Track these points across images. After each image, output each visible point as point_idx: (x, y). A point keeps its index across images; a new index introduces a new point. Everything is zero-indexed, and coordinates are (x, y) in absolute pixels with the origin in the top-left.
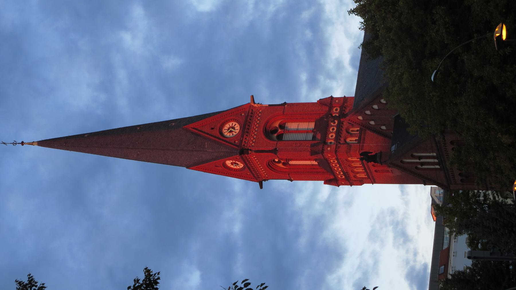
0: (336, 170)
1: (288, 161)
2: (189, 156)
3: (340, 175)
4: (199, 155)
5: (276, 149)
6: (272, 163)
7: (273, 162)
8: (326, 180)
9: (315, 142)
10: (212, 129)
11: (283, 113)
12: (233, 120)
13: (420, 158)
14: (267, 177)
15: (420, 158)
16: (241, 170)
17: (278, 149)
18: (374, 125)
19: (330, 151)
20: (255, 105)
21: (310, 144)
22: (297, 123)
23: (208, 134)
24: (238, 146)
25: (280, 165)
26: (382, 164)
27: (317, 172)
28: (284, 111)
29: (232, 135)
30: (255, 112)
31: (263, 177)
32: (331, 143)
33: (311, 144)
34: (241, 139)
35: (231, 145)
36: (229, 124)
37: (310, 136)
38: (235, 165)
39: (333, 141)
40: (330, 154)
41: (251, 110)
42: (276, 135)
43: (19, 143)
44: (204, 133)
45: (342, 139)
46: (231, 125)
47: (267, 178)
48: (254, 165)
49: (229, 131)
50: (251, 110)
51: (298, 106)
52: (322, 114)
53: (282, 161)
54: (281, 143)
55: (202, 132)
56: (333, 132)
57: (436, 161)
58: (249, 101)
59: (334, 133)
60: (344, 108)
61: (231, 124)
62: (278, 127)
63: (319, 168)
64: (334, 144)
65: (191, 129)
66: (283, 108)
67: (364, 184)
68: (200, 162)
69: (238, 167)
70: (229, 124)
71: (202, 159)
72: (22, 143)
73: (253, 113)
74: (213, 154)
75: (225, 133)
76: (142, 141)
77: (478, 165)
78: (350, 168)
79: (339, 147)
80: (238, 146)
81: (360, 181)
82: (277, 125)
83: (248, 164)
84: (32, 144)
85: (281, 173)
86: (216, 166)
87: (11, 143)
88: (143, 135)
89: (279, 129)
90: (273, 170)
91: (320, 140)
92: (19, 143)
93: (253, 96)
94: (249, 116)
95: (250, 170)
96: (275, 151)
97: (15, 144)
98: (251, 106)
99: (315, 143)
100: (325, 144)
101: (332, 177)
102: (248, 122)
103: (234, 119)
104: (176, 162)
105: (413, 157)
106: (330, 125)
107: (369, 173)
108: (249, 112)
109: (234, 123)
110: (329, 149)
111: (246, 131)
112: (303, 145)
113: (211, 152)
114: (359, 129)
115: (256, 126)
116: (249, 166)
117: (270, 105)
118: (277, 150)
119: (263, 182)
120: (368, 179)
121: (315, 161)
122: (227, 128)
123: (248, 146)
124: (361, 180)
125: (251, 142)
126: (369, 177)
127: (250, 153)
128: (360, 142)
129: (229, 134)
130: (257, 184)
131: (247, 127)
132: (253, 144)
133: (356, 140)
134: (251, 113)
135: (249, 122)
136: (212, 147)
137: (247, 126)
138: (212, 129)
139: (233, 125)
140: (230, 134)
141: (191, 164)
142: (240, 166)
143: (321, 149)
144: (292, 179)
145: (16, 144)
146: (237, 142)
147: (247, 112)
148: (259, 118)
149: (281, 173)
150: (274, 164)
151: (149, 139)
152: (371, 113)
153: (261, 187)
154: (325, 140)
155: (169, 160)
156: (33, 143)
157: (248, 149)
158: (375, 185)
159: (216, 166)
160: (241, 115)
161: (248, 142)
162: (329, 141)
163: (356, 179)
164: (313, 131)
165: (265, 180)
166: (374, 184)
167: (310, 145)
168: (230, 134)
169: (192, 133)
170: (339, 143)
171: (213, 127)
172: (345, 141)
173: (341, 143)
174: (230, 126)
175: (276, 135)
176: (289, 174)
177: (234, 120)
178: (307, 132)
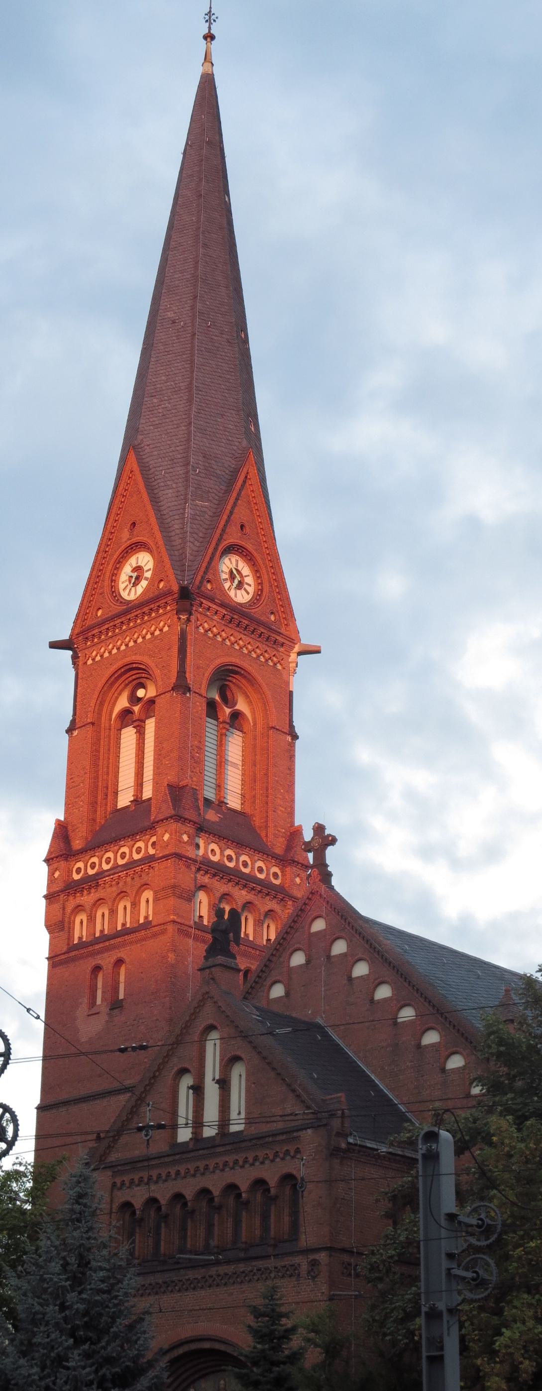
0: (90, 861)
1: (136, 724)
2: (171, 454)
3: (80, 869)
4: (173, 480)
5: (189, 690)
6: (135, 679)
7: (135, 682)
8: (66, 828)
9: (201, 803)
10: (242, 527)
11: (273, 728)
12: (260, 587)
13: (224, 1084)
14: (86, 663)
15: (224, 1084)
16: (113, 592)
17: (188, 695)
18: (289, 962)
19: (180, 841)
20: (293, 656)
21: (197, 788)
22: (240, 763)
23: (231, 513)
24: (199, 588)
25: (123, 702)
26: (200, 970)
27: (96, 803)
28: (277, 729)
29: (224, 578)
30: (278, 651)
31: (86, 651)
32: (198, 846)
33: (196, 789)
34: (216, 600)
35: (203, 569)
36: (249, 576)
37: (209, 793)
38: (131, 577)
39: (201, 852)
40: (170, 838)
41: (283, 640)
42: (217, 698)
43: (210, 28)
44: (235, 504)
45: (206, 880)
46: (247, 580)
47: (81, 663)
48: (111, 637)
49: (235, 572)
50: (283, 640)
51: (288, 772)
52: (267, 836)
53: (136, 709)
54: (201, 706)
55: (237, 499)
56: (224, 856)
57: (209, 1132)
58: (306, 638)
59: (238, 856)
60: (280, 896)
61: (249, 580)
62: (235, 708)
63: (106, 809)
64: (197, 855)
65: (245, 470)
66: (285, 731)
67: (50, 932)
68: (150, 480)
69: (122, 586)
70: (249, 576)
71: (162, 488)
72: (209, 37)
73: (274, 646)
74: (177, 517)
75: (230, 559)
76: (215, 338)
77: (508, 1213)
78: (114, 895)
79: (188, 867)
80: (199, 588)
81: (62, 922)
82: (242, 705)
83: (112, 624)
84: (207, 58)
85: (98, 702)
86: (134, 524)
87: (210, 8)
88: (230, 342)
89: (230, 710)
90: (110, 682)
91: (204, 818)
92: (210, 28)
93: (318, 652)
94: (269, 633)
95: (112, 619)
96: (181, 686)
97: (213, 17)
98: (293, 645)
99: (199, 802)
100: (199, 828)
101: (77, 844)
102: (256, 627)
103: (262, 590)
104: (151, 420)
105: (229, 1061)
106: (241, 852)
107: (91, 948)
108: (280, 634)
109: (251, 590)
110: (185, 838)
111: (235, 617)
112: (195, 768)
113: (184, 514)
114: (205, 922)
115: (244, 649)
116: (133, 615)
117: (291, 693)
118: (185, 693)
119: (70, 653)
120: (68, 944)
121: (132, 799)
122: (240, 568)
123: (199, 617)
124: (66, 924)
125: (206, 625)
126: (72, 948)
127: (179, 618)
128: (199, 930)
129: (227, 570)
130: (65, 635)
131: (244, 621)
132: (201, 630)
133: (247, 935)
134: (276, 639)
135: (255, 629)
136: (198, 517)
137: (246, 622)
138: (242, 527)
139: (246, 586)
140: (226, 573)
141: (144, 457)
142: (128, 590)
143: (187, 815)
144: (75, 733)
145: (207, 21)
146: (209, 586)
147: (279, 628)
148: (262, 659)
149: (98, 702)
150: (127, 685)
151: (218, 356)
152: (335, 956)
153: (54, 645)
154: (206, 832)
155: (155, 401)
156: (211, 64)
157: (190, 614)
158: (45, 964)
159: (134, 524)
160: (272, 613)
161: (207, 616)
162: (201, 843)
163: (69, 910)
164: (222, 803)
165: (75, 658)
166: (46, 962)
167: (195, 787)
168: (226, 573)
169: (235, 472)
170: (199, 870)
171: (247, 530)
172: (203, 887)
173: (198, 875)
174: (246, 576)
175: (217, 698)
176: (93, 724)
177: (259, 584)
178: (220, 787)
